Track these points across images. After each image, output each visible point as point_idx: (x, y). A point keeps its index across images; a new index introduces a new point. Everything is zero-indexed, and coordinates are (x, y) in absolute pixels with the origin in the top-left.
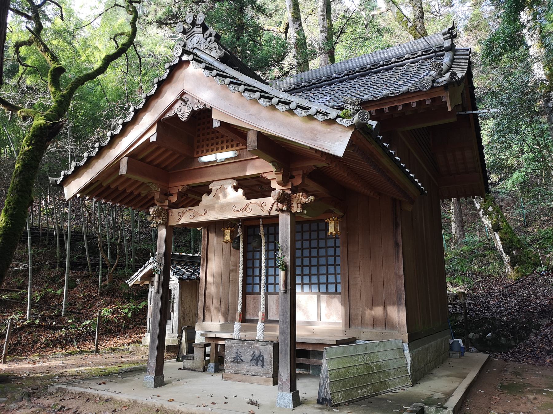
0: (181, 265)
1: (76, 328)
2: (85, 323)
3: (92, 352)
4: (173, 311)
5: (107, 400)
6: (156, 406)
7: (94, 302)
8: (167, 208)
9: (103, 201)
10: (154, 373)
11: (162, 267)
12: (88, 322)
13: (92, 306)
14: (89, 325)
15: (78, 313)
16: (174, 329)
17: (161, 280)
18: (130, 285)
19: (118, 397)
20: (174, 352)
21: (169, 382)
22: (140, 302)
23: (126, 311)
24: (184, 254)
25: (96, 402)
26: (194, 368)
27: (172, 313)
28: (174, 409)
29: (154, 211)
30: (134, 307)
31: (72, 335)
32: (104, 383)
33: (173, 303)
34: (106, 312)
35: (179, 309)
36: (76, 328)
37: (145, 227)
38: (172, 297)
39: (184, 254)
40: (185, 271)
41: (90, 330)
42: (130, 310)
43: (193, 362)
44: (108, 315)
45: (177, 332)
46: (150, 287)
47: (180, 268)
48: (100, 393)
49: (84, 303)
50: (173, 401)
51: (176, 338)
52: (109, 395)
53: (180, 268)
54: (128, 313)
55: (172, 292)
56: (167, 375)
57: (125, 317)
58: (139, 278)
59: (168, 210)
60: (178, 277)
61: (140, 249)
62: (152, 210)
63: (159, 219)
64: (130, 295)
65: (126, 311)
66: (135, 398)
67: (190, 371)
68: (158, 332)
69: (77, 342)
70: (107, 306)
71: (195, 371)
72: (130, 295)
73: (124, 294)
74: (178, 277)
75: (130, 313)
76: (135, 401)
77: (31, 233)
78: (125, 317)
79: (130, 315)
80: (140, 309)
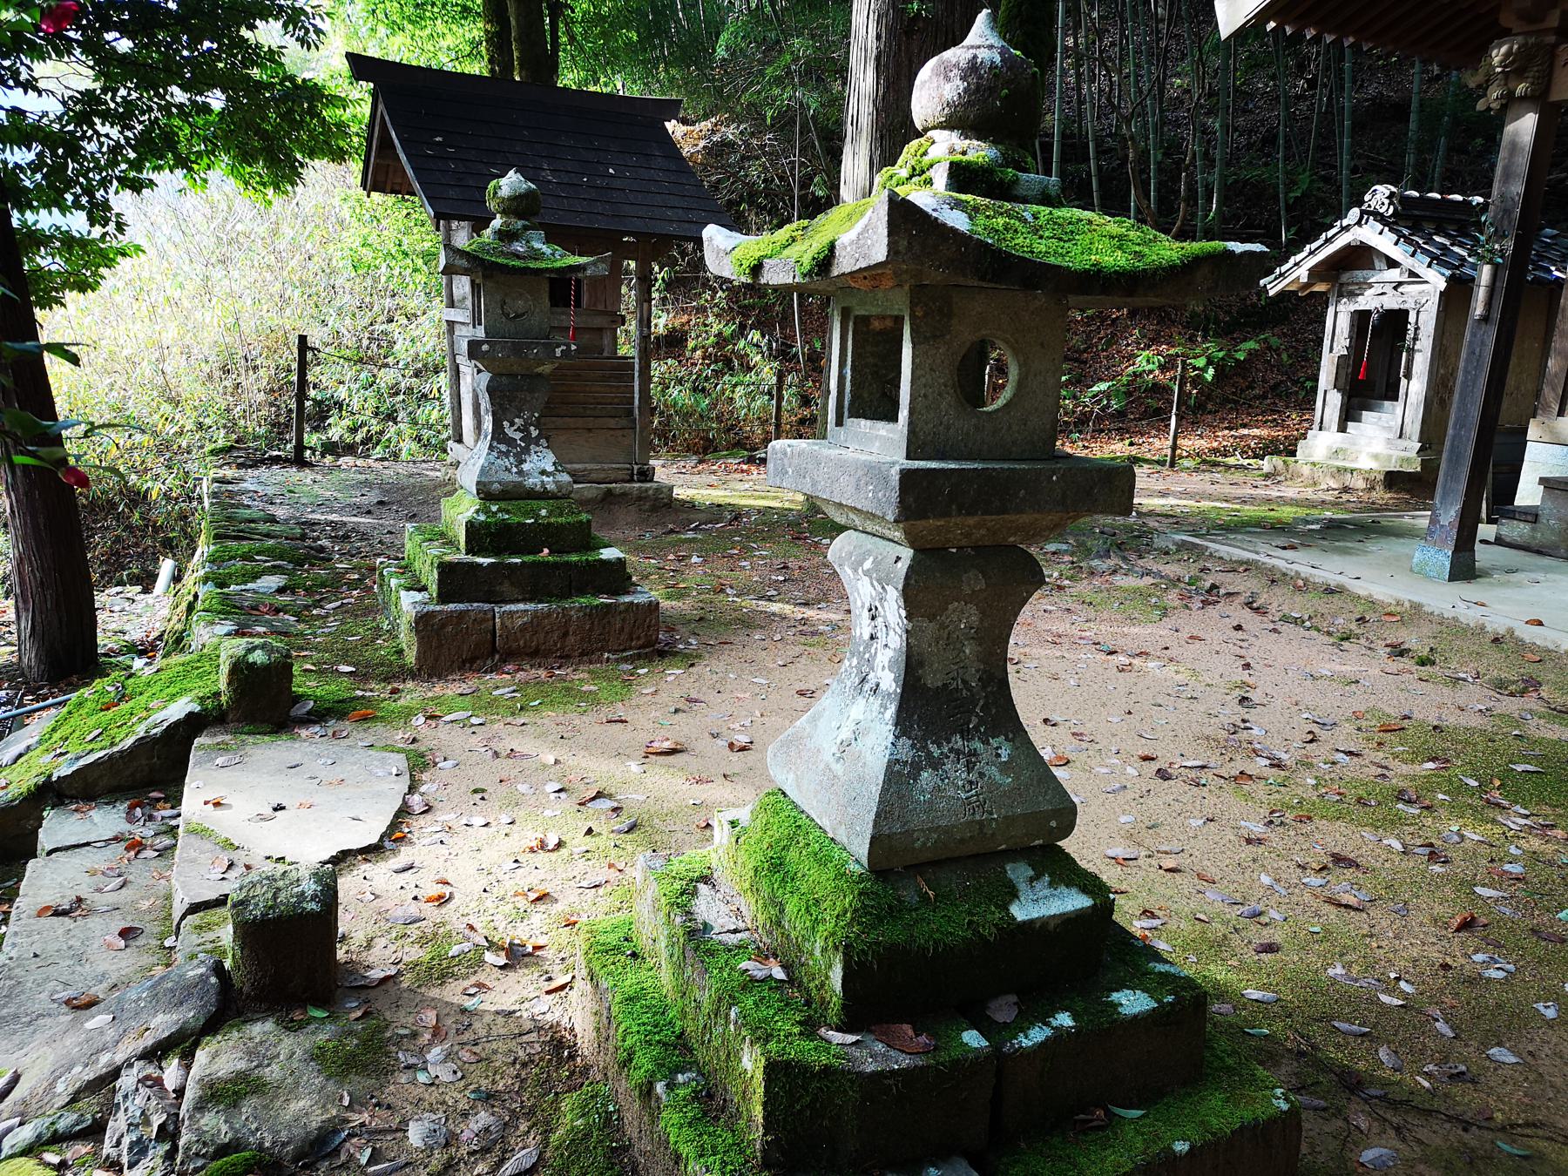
0: (1447, 236)
1: (1075, 397)
2: (1095, 389)
3: (1161, 463)
4: (1408, 376)
5: (1329, 591)
6: (1489, 629)
7: (1113, 335)
8: (1551, 39)
9: (1310, 33)
10: (1452, 544)
11: (1509, 245)
12: (1103, 386)
13: (1109, 344)
14: (1107, 394)
15: (1076, 360)
16: (1407, 429)
17: (1503, 284)
18: (1271, 293)
19: (1360, 588)
20: (1408, 492)
21: (1484, 574)
22: (1236, 343)
23: (1201, 362)
24: (1459, 198)
25: (1299, 589)
26: (1533, 543)
27: (1404, 382)
28: (1552, 647)
29: (1508, 54)
30: (1221, 354)
31: (1066, 414)
32: (1293, 548)
33: (1411, 351)
34: (1146, 362)
35: (1430, 372)
36: (1075, 397)
37: (1245, 111)
38: (1411, 334)
39: (1459, 198)
40: (1464, 253)
41: (1108, 406)
42: (1210, 362)
43: (1533, 529)
44: (1151, 372)
45: (1416, 436)
46: (1332, 300)
47: (1447, 243)
48: (1305, 571)
49: (1089, 338)
50: (1540, 623)
51: (1413, 454)
52: (1333, 579)
53: (1447, 243)
54: (1204, 370)
55: (1412, 318)
56: (1484, 555)
57: (1197, 381)
58: (1302, 274)
59: (1556, 46)
60: (1448, 273)
61: (1236, 181)
62: (1504, 49)
63: (1522, 79)
64: (1207, 318)
65: (1201, 362)
66: (1416, 599)
67: (1522, 553)
68: (1473, 435)
69: (1080, 432)
70: (1147, 347)
71: (1539, 552)
72: (1207, 318)
73: (1194, 315)
74: (1448, 273)
75: (1211, 371)
76: (1416, 607)
77: (1063, 146)
78: (1197, 381)
79: (1210, 374)
80: (1237, 360)
